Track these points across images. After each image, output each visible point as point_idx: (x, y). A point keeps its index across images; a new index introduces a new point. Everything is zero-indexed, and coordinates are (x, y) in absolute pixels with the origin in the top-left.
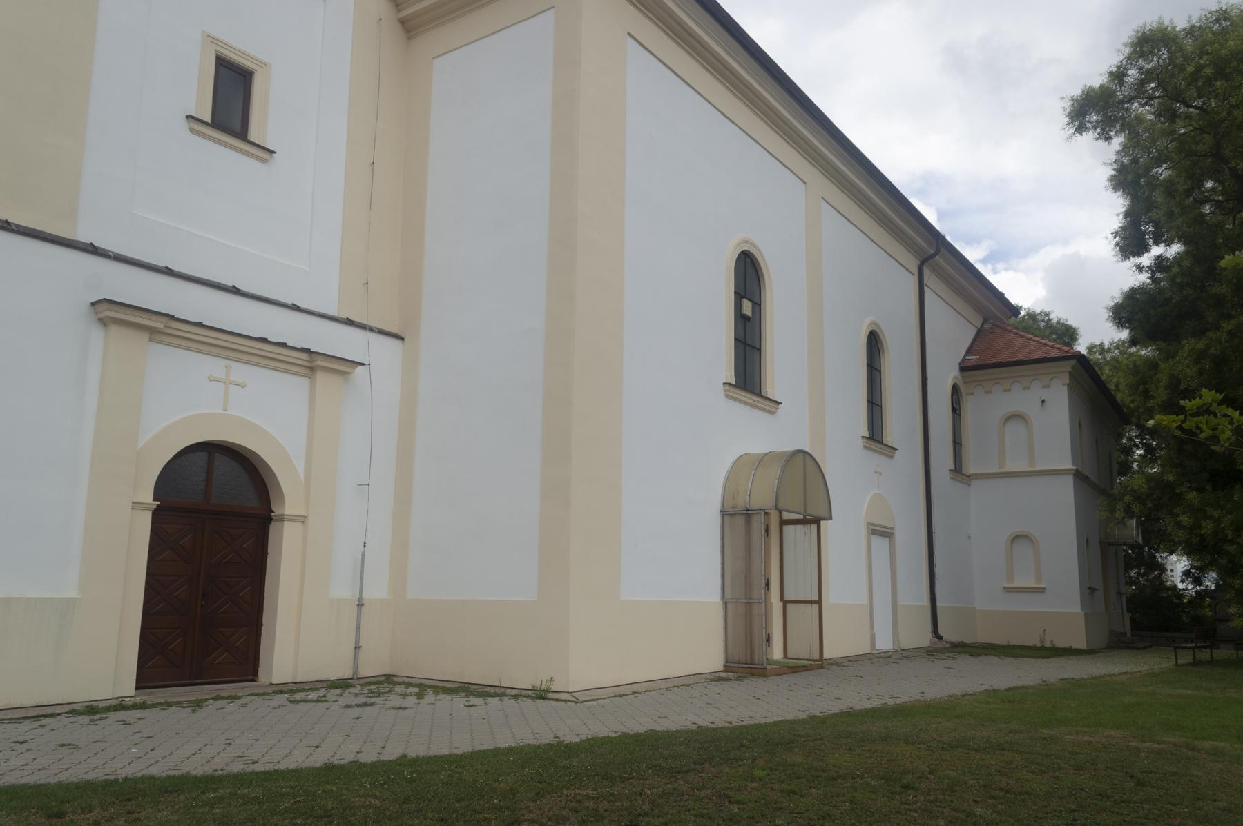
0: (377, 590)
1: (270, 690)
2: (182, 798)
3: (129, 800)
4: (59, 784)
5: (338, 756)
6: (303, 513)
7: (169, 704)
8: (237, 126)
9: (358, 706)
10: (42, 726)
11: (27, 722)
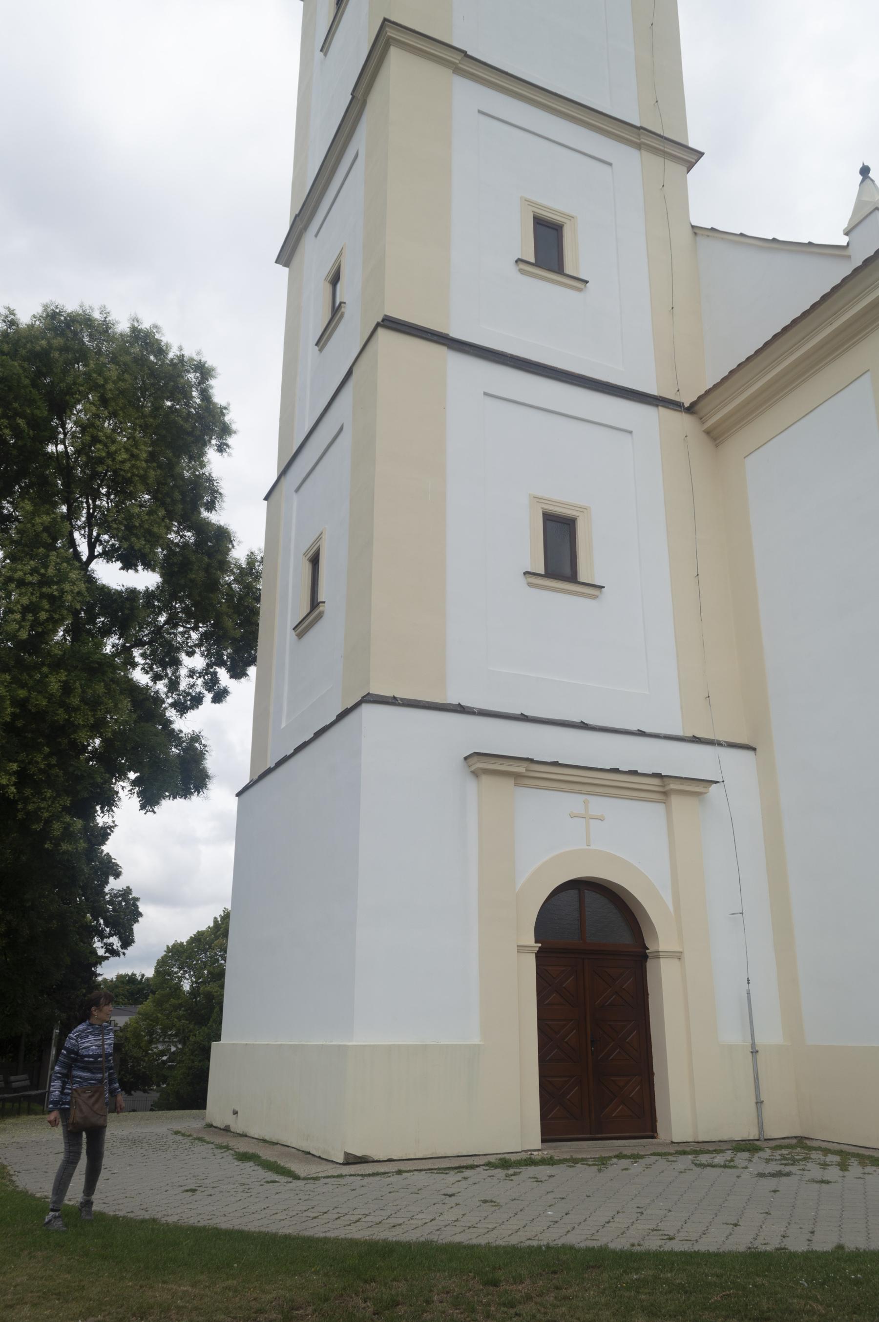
0: (771, 1035)
1: (672, 1150)
2: (605, 1276)
3: (555, 1272)
4: (488, 1246)
5: (760, 1240)
6: (677, 948)
7: (575, 1161)
8: (568, 571)
9: (773, 1175)
10: (465, 1178)
11: (452, 1172)
